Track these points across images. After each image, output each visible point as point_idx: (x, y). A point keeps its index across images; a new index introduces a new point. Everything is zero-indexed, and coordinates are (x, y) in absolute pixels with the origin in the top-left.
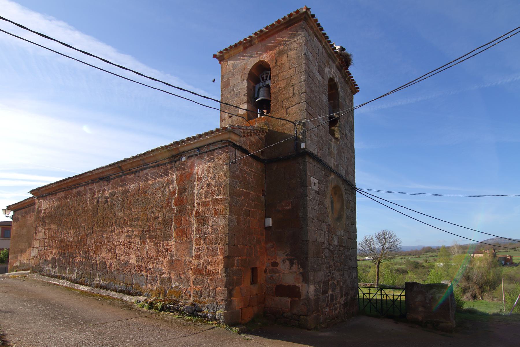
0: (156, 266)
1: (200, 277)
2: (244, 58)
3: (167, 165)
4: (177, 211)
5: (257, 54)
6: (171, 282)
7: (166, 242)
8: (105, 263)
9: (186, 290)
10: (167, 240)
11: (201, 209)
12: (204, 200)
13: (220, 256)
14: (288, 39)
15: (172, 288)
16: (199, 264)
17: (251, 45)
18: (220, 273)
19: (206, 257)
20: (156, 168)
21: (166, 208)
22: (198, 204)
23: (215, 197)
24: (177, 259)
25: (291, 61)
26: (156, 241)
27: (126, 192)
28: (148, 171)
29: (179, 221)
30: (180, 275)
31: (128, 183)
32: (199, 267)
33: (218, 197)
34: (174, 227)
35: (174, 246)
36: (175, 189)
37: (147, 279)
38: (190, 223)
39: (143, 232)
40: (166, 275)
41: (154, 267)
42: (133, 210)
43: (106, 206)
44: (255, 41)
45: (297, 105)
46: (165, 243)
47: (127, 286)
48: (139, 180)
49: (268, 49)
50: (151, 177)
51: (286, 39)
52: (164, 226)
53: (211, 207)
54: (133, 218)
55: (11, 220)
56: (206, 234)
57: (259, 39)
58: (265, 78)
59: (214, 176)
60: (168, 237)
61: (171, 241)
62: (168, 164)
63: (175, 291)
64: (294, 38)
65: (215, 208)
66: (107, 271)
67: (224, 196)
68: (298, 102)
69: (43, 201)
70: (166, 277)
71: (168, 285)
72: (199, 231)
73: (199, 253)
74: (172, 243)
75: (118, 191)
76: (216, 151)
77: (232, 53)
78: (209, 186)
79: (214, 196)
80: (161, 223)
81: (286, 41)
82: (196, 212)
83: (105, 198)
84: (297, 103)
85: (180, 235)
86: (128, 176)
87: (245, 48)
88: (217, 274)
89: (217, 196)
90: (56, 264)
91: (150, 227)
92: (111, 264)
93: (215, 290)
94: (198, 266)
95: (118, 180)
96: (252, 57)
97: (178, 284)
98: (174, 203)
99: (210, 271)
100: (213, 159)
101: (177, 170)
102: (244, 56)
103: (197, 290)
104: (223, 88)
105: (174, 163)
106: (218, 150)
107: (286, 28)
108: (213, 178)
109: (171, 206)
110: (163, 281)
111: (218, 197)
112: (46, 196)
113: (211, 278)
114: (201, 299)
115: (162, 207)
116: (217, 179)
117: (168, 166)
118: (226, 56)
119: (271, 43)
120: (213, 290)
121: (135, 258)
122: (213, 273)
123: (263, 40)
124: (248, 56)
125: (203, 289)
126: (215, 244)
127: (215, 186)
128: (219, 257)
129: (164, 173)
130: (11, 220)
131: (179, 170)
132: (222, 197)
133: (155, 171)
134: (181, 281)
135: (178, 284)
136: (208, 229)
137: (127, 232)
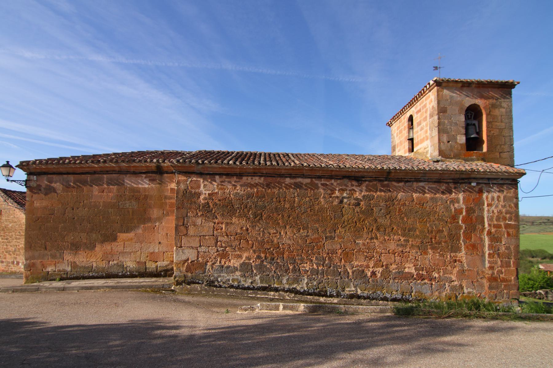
0: (443, 274)
1: (494, 284)
2: (460, 94)
3: (450, 184)
4: (466, 228)
5: (473, 96)
6: (462, 288)
7: (454, 254)
8: (363, 271)
9: (481, 294)
10: (456, 252)
11: (493, 230)
12: (495, 223)
13: (513, 267)
14: (500, 98)
15: (464, 293)
16: (493, 273)
17: (468, 87)
18: (513, 280)
19: (500, 268)
20: (436, 183)
21: (452, 224)
22: (489, 225)
23: (507, 222)
24: (469, 269)
25: (502, 117)
26: (441, 252)
27: (391, 200)
28: (425, 184)
29: (468, 237)
30: (472, 282)
31: (395, 191)
32: (494, 276)
33: (509, 223)
34: (463, 242)
35: (464, 258)
36: (462, 209)
37: (432, 287)
38: (482, 240)
39: (422, 242)
40: (456, 283)
41: (440, 276)
42: (405, 219)
43: (357, 209)
44: (473, 85)
45: (508, 153)
46: (452, 254)
47: (403, 295)
48: (411, 191)
49: (482, 97)
50: (428, 190)
51: (498, 97)
52: (451, 240)
53: (504, 229)
54: (406, 228)
55: (24, 189)
56: (498, 250)
57: (477, 86)
58: (470, 117)
59: (505, 205)
60: (458, 250)
61: (459, 253)
62: (452, 184)
63: (468, 296)
64: (504, 99)
65: (507, 231)
66: (368, 280)
67: (515, 222)
68: (508, 150)
69: (203, 182)
70: (457, 284)
71: (460, 291)
72: (492, 247)
73: (493, 265)
74: (462, 255)
75: (377, 197)
76: (505, 185)
77: (451, 84)
78: (500, 212)
79: (506, 221)
80: (447, 237)
81: (498, 98)
82: (488, 232)
83: (354, 199)
84: (508, 152)
85: (471, 249)
86: (395, 184)
87: (463, 86)
88: (511, 281)
89: (509, 221)
90: (252, 271)
91: (431, 239)
92: (374, 274)
93: (509, 293)
94: (492, 275)
95: (376, 184)
96: (468, 97)
97: (471, 290)
98: (461, 221)
99: (503, 278)
100: (503, 191)
101: (464, 191)
102: (461, 93)
103: (492, 294)
104: (440, 113)
105: (459, 185)
106: (508, 185)
107: (499, 88)
108: (504, 206)
109: (458, 222)
110: (453, 288)
111: (509, 223)
112: (214, 174)
113: (505, 284)
114: (496, 300)
115: (446, 222)
116: (508, 208)
117: (452, 185)
118: (444, 84)
119: (486, 94)
120: (507, 293)
121: (414, 268)
122: (507, 280)
123: (479, 87)
124: (465, 95)
125: (498, 293)
126: (508, 258)
127: (506, 213)
128: (512, 268)
129: (445, 190)
130: (24, 189)
131: (466, 192)
132: (513, 223)
133: (434, 186)
134: (475, 287)
135: (471, 290)
136: (501, 246)
137: (398, 241)
